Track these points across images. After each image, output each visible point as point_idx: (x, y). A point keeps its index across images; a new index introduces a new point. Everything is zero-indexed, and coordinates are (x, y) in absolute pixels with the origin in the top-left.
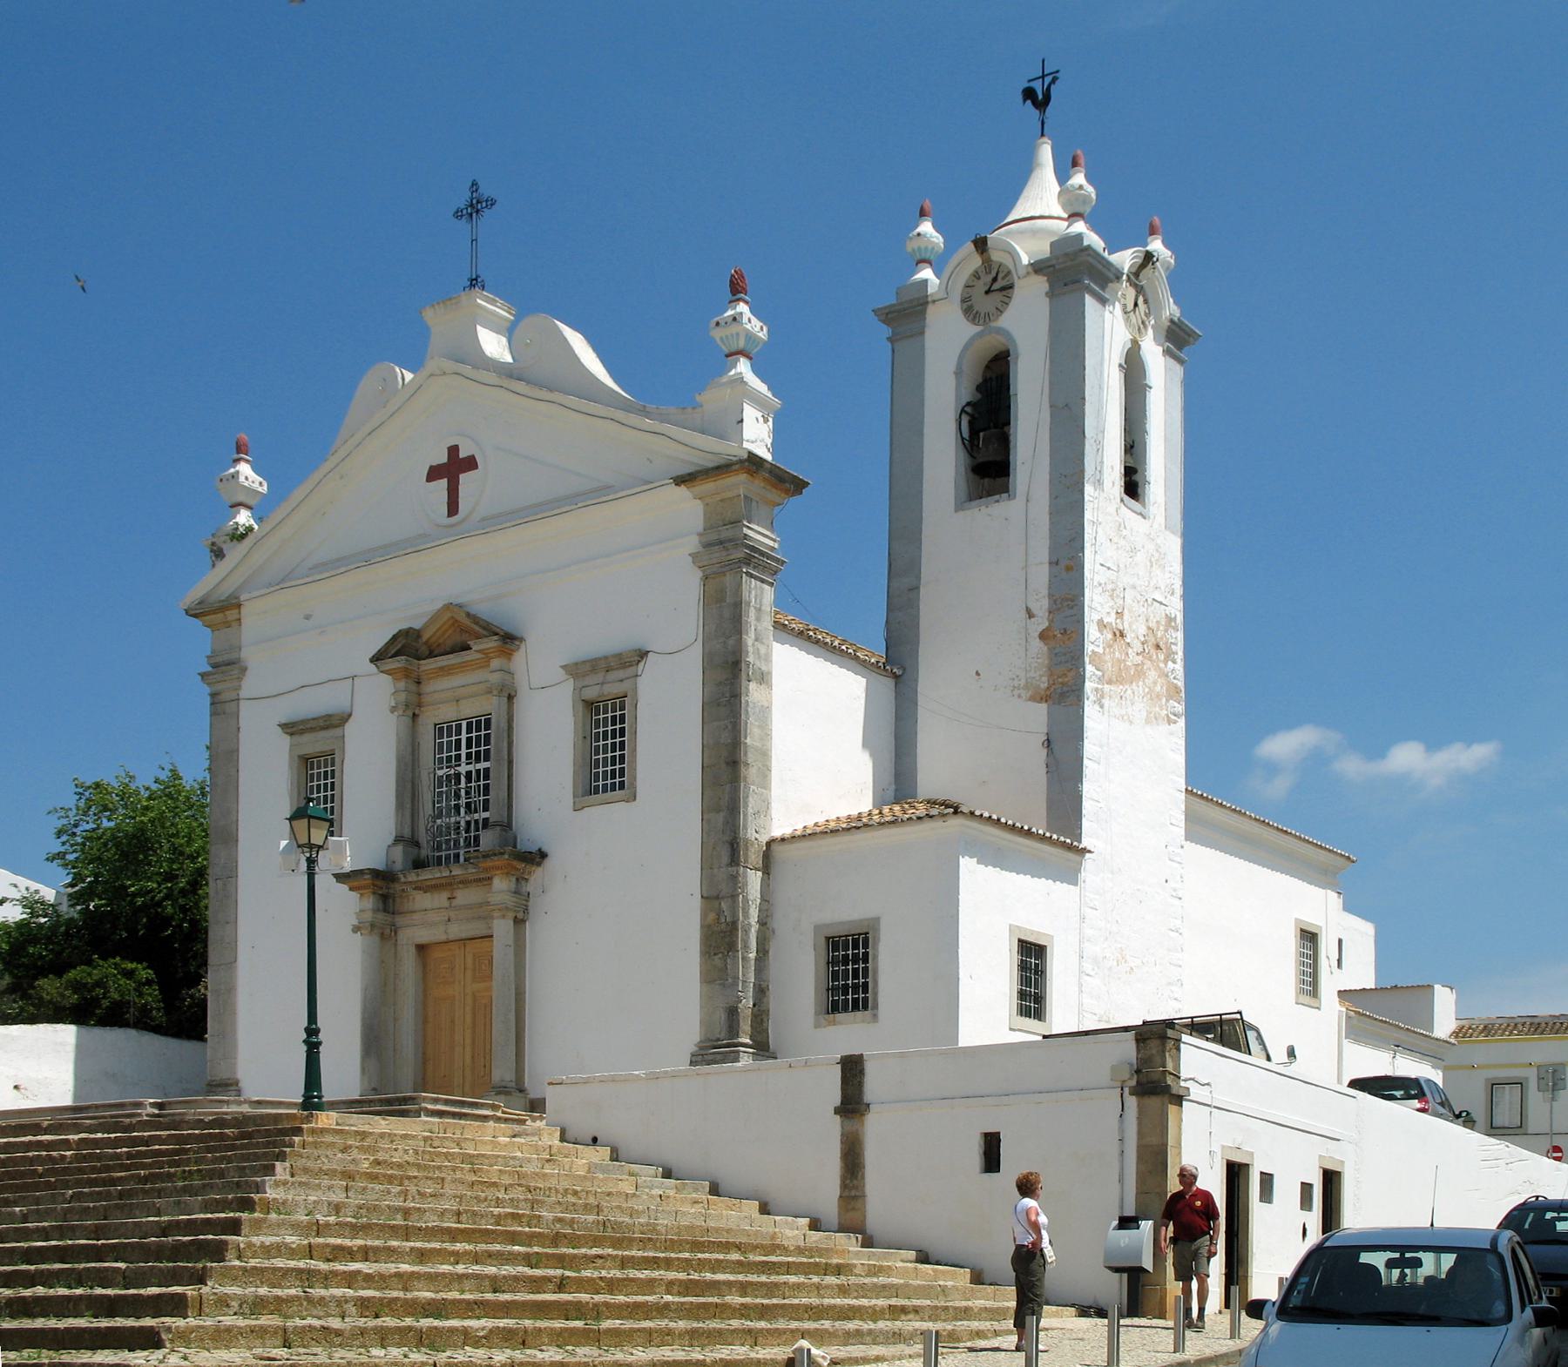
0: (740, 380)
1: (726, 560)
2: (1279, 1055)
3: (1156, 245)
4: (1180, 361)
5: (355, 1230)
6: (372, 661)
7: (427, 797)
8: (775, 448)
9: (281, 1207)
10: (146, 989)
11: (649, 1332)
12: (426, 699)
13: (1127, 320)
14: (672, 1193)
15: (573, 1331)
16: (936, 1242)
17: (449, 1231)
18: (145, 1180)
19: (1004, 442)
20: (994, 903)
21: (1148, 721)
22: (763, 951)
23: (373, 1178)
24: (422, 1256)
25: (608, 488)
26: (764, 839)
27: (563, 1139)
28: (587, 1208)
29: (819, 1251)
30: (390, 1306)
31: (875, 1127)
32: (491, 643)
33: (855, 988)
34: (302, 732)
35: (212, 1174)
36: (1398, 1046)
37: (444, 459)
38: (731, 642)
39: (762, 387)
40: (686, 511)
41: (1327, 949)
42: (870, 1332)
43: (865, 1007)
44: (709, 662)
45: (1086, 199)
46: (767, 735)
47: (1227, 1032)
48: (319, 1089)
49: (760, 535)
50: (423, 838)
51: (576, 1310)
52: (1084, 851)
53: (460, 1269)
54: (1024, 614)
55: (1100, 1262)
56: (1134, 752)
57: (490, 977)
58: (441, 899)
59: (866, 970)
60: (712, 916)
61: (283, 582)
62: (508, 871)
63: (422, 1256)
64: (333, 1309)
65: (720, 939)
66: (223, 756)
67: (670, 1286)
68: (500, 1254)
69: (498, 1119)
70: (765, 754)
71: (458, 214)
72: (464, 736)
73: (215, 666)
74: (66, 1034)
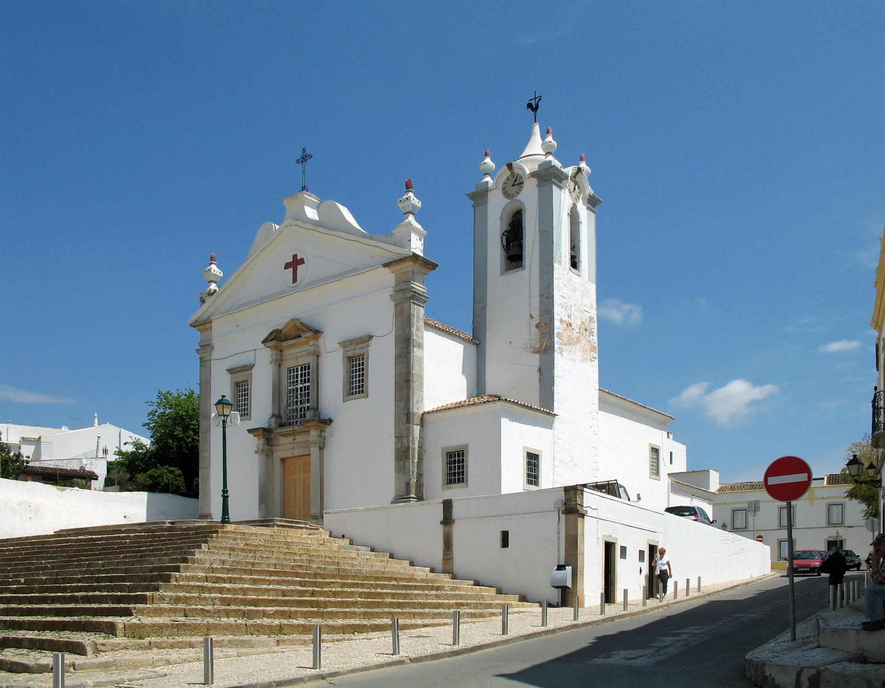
0: (410, 223)
1: (405, 297)
2: (633, 498)
3: (583, 165)
4: (594, 212)
5: (228, 571)
7: (284, 398)
8: (425, 250)
9: (200, 561)
10: (178, 478)
11: (346, 613)
12: (284, 358)
13: (571, 196)
14: (372, 557)
15: (312, 612)
16: (483, 577)
17: (269, 571)
18: (153, 551)
19: (521, 246)
20: (516, 437)
21: (582, 361)
22: (420, 459)
23: (243, 550)
24: (255, 581)
25: (356, 270)
26: (421, 412)
27: (330, 536)
28: (333, 563)
29: (432, 581)
30: (235, 601)
31: (457, 530)
32: (310, 334)
34: (235, 372)
35: (177, 548)
36: (693, 495)
37: (291, 260)
38: (406, 331)
39: (419, 227)
40: (388, 277)
41: (664, 456)
42: (444, 613)
44: (398, 340)
45: (553, 147)
46: (421, 369)
47: (610, 488)
48: (228, 515)
49: (418, 287)
50: (283, 415)
51: (317, 604)
52: (555, 415)
53: (271, 587)
54: (529, 317)
55: (549, 584)
56: (576, 374)
57: (310, 471)
58: (290, 439)
59: (463, 466)
60: (399, 445)
61: (228, 312)
62: (317, 427)
63: (255, 581)
64: (210, 602)
65: (402, 454)
66: (205, 383)
67: (361, 595)
68: (288, 581)
69: (307, 528)
70: (421, 377)
71: (298, 162)
73: (202, 347)
74: (144, 495)
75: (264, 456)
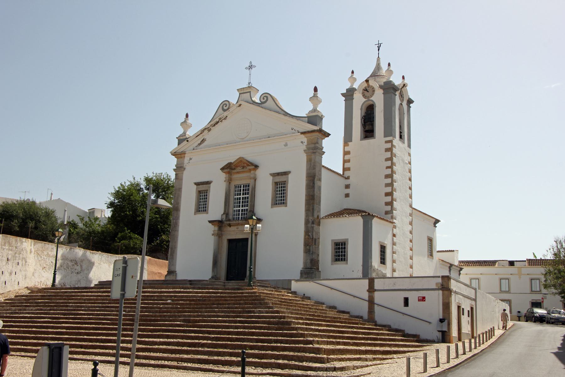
6: (221, 169)
33: (342, 255)
43: (344, 260)
59: (345, 251)
71: (246, 68)
72: (242, 189)
75: (217, 238)
